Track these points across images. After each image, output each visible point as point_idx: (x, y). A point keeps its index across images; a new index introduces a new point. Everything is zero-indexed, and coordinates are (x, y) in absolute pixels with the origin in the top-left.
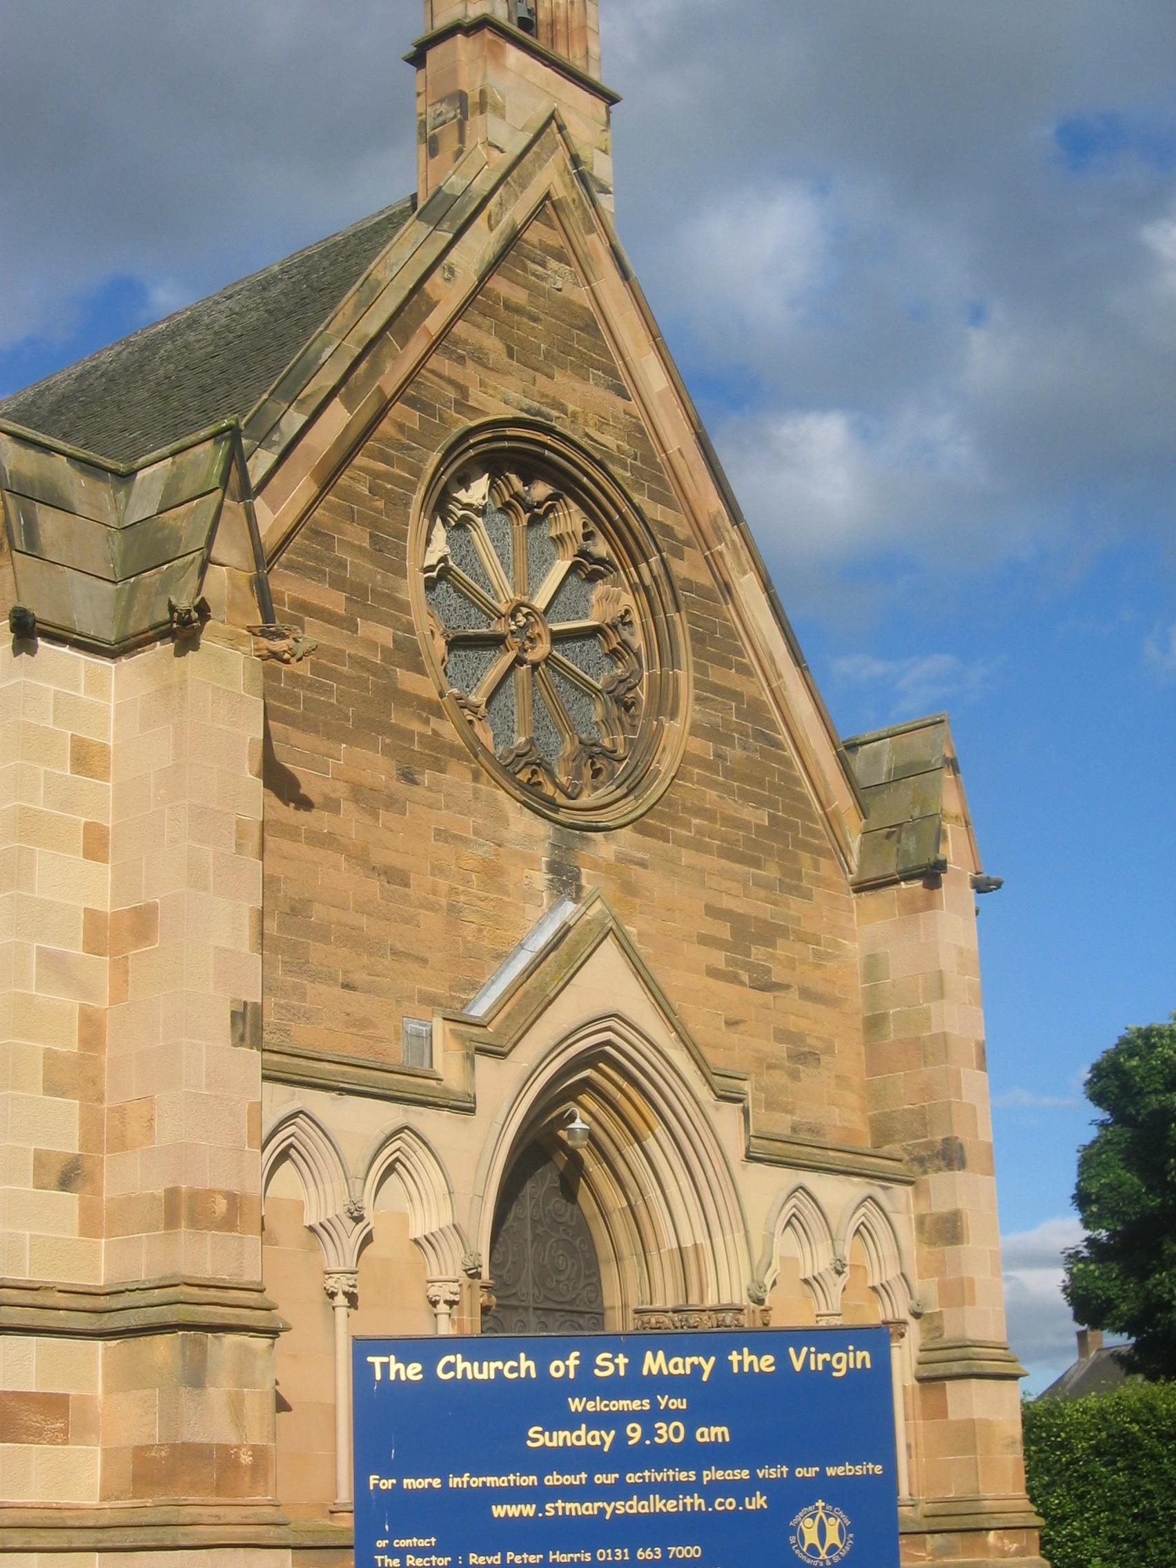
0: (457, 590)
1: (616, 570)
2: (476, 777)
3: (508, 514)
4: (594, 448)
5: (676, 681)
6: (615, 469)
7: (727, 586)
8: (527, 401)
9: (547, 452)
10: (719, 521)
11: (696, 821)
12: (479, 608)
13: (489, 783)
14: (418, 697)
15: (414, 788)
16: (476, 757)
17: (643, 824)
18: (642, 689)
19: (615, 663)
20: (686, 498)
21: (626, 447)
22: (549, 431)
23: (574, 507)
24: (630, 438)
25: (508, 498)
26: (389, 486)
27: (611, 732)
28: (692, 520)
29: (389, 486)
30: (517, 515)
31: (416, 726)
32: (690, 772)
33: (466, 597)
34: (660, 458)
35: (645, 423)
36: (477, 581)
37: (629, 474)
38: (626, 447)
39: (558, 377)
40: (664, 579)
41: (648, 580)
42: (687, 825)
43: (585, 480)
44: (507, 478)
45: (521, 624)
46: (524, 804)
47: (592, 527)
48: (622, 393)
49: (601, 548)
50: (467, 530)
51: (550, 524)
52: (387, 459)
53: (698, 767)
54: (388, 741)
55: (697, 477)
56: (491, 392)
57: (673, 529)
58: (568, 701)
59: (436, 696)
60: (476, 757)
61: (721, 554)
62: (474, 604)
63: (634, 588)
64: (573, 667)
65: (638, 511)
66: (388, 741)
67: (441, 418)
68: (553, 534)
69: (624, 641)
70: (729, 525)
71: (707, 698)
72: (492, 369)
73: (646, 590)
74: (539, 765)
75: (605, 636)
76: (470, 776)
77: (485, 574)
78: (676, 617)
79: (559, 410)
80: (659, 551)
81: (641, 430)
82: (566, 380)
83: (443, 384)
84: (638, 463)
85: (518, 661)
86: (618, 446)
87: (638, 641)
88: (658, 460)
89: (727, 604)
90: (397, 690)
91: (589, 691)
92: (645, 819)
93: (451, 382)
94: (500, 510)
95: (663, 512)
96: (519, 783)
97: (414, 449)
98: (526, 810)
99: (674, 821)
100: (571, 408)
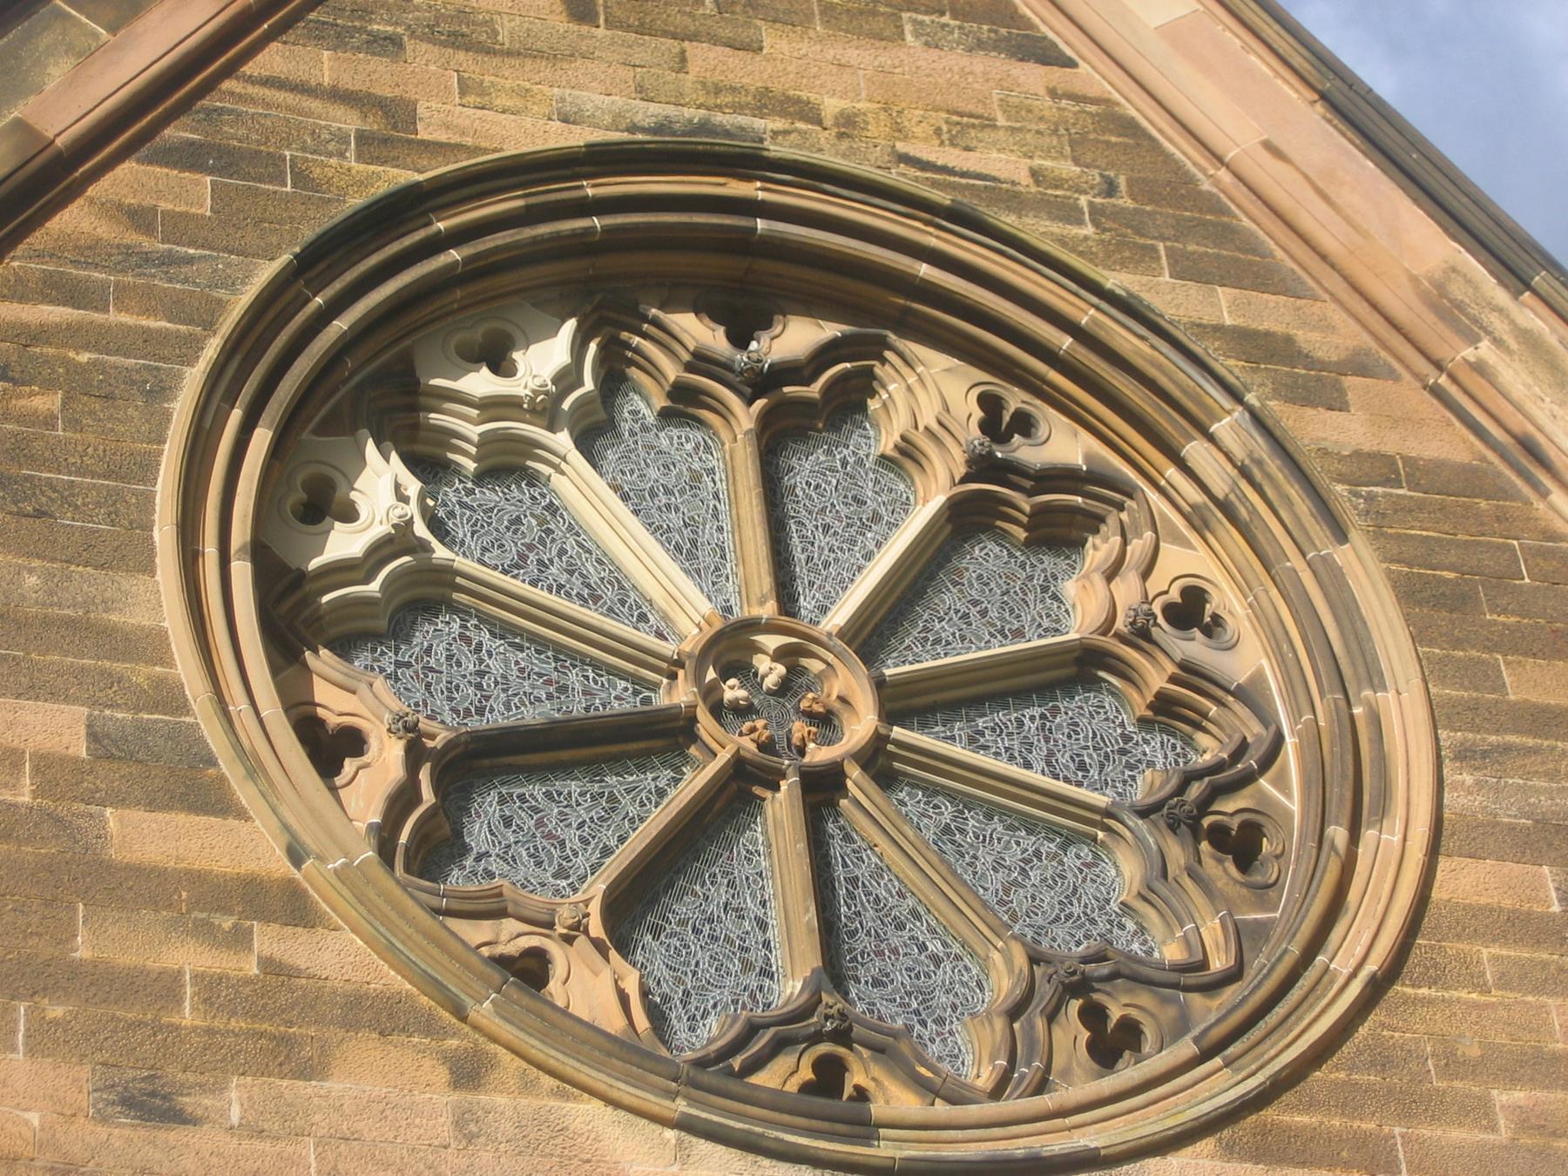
0: (503, 631)
1: (1129, 491)
2: (468, 1073)
3: (701, 422)
4: (935, 184)
5: (1375, 720)
6: (1037, 229)
7: (1529, 447)
8: (654, 108)
9: (761, 224)
10: (1457, 290)
11: (1503, 1097)
12: (596, 665)
13: (527, 1087)
14: (196, 878)
15: (175, 1135)
16: (460, 1013)
17: (1264, 1131)
18: (1282, 783)
19: (1188, 741)
20: (1324, 257)
21: (1068, 169)
22: (749, 163)
23: (935, 361)
24: (1078, 147)
25: (1025, 503)
26: (84, 357)
27: (1175, 916)
28: (1362, 309)
29: (84, 357)
30: (724, 412)
31: (189, 958)
32: (1465, 962)
33: (542, 644)
34: (1212, 180)
35: (1135, 107)
36: (592, 598)
37: (1089, 230)
38: (1068, 169)
39: (774, 41)
40: (1274, 465)
41: (1219, 476)
42: (1481, 1112)
43: (924, 270)
44: (656, 323)
45: (770, 682)
46: (686, 1125)
47: (1016, 399)
48: (1048, 55)
49: (1062, 444)
50: (533, 479)
51: (876, 427)
52: (73, 294)
53: (1501, 937)
54: (57, 1012)
55: (1348, 198)
56: (503, 101)
57: (1289, 340)
58: (998, 865)
59: (280, 866)
60: (460, 1013)
61: (1479, 368)
62: (573, 654)
63: (1198, 522)
64: (1015, 771)
65: (1128, 307)
66: (57, 1012)
67: (301, 179)
68: (887, 443)
69: (1185, 666)
70: (1501, 296)
71: (1507, 749)
72: (509, 53)
73: (1225, 507)
74: (843, 1036)
75: (1125, 672)
76: (442, 1074)
77: (620, 581)
78: (1342, 555)
79: (783, 114)
80: (1237, 397)
81: (1129, 127)
82: (783, 45)
83: (315, 105)
84: (1125, 202)
85: (822, 789)
86: (1034, 173)
87: (1247, 658)
88: (1206, 186)
89: (1544, 494)
90: (106, 868)
91: (1081, 828)
92: (1270, 1114)
93: (337, 95)
94: (666, 416)
95: (1234, 306)
96: (774, 1101)
97: (190, 260)
98: (703, 1146)
99: (1413, 1105)
100: (831, 106)
